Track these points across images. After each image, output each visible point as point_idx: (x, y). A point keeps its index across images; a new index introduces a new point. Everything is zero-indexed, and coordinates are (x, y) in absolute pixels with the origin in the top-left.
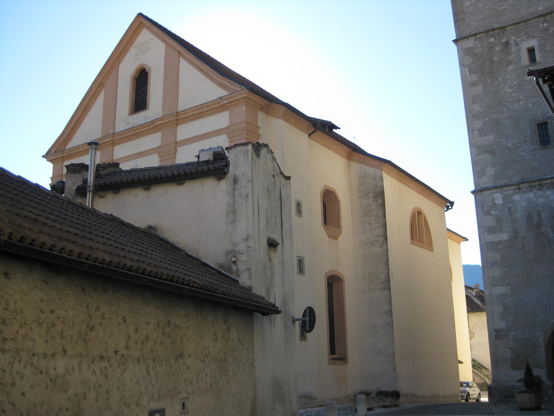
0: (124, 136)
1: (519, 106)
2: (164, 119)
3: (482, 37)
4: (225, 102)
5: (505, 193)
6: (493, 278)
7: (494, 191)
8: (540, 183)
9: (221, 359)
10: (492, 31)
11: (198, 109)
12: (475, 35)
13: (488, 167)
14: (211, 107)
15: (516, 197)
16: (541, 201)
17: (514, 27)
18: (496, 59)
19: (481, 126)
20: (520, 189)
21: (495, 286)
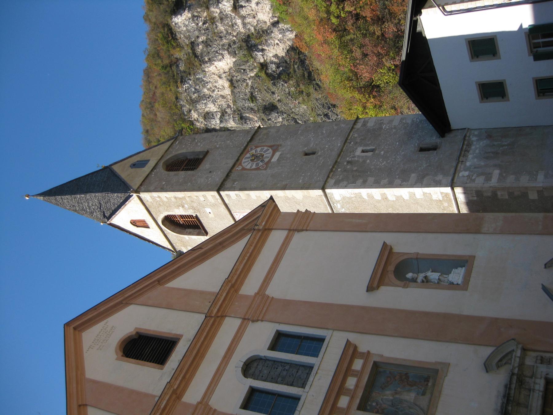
0: (184, 371)
1: (400, 159)
2: (219, 299)
3: (332, 174)
4: (263, 224)
5: (462, 169)
6: (529, 180)
7: (457, 175)
8: (464, 151)
9: (383, 389)
10: (333, 168)
11: (245, 256)
12: (328, 177)
13: (435, 179)
14: (255, 242)
15: (468, 164)
16: (477, 151)
17: (340, 158)
18: (355, 169)
19: (400, 180)
20: (463, 161)
21: (536, 179)
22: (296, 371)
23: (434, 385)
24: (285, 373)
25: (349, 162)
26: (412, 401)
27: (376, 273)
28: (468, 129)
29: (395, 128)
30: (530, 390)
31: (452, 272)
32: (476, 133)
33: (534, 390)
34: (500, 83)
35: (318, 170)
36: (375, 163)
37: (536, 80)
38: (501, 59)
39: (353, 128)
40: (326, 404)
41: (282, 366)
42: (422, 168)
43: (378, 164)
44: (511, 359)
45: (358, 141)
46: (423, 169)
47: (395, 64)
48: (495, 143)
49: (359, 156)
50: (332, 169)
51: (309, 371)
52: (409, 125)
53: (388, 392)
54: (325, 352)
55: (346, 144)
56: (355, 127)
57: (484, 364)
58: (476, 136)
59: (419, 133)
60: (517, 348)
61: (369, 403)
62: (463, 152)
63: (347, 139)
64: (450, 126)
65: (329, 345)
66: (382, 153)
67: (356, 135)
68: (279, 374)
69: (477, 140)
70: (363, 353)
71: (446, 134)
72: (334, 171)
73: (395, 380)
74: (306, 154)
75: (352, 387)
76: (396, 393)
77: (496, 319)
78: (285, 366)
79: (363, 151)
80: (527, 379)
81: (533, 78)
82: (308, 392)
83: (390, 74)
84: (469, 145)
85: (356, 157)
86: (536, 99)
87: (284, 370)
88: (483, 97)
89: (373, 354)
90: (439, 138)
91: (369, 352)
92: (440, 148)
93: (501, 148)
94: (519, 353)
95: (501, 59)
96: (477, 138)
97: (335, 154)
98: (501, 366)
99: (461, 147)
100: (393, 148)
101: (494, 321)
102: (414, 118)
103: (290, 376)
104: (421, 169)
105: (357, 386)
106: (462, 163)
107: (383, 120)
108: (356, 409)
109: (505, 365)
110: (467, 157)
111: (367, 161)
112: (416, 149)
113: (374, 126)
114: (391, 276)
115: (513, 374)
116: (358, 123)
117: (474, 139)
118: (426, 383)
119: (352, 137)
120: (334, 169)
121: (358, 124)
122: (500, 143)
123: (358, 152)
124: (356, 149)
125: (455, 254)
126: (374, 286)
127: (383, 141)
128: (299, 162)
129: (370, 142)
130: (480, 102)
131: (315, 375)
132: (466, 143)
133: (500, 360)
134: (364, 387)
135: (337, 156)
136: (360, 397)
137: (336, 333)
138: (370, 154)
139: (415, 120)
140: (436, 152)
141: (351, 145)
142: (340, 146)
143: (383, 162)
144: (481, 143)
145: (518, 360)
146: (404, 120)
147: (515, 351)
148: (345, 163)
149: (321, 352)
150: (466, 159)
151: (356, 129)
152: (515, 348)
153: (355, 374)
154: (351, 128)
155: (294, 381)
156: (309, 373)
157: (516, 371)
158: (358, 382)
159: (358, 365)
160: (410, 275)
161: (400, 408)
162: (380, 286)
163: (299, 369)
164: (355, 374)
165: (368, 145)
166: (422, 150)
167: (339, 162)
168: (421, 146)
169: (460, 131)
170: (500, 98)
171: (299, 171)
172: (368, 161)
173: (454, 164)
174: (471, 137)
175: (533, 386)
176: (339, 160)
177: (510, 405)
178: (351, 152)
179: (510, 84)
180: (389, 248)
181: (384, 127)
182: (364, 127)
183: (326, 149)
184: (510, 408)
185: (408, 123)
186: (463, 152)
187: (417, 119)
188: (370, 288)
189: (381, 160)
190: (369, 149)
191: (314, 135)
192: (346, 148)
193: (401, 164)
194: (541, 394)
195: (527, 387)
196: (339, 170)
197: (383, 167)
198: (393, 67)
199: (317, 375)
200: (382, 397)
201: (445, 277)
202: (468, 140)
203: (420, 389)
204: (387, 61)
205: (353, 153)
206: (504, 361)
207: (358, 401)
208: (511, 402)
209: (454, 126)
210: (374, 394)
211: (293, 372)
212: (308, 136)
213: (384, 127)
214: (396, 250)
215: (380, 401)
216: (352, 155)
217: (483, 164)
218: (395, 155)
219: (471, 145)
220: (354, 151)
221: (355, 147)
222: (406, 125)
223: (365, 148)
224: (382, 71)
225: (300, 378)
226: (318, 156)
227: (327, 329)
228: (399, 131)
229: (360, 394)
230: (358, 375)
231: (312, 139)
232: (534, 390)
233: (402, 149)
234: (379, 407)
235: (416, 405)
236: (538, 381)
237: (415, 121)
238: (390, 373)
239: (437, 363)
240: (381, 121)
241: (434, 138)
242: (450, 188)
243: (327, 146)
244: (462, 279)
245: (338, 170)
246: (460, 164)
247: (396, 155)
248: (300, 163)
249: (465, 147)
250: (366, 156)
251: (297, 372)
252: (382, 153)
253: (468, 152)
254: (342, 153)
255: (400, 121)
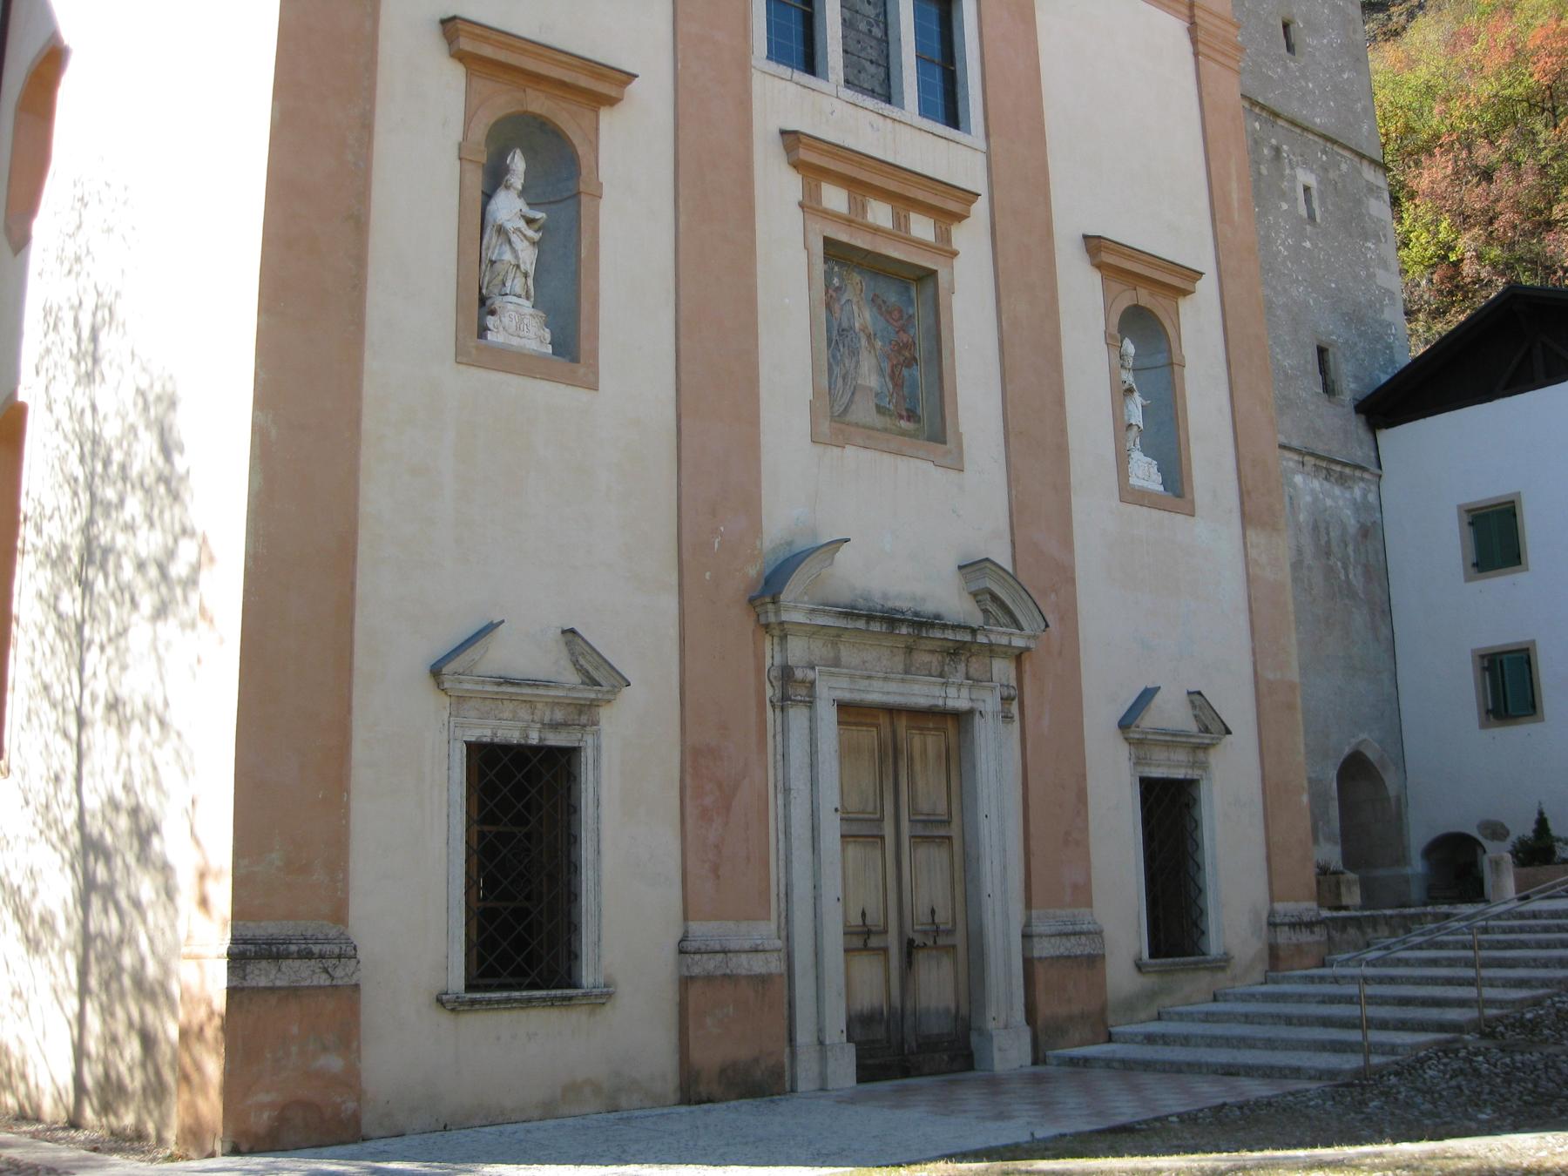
9: (873, 300)
16: (1329, 502)
17: (1286, 125)
18: (1264, 171)
22: (874, 59)
23: (903, 433)
24: (863, 26)
25: (1277, 150)
27: (1133, 257)
28: (1380, 476)
29: (1371, 276)
30: (941, 675)
31: (1149, 460)
32: (1372, 498)
33: (945, 684)
34: (1519, 556)
35: (1250, 64)
36: (1282, 224)
37: (1528, 649)
39: (1362, 156)
40: (828, 152)
41: (878, 15)
42: (1279, 357)
43: (1281, 235)
44: (998, 623)
45: (1332, 175)
46: (1278, 360)
47: (1465, 262)
48: (1350, 549)
49: (1294, 178)
50: (1256, 105)
51: (878, 94)
52: (1378, 316)
53: (867, 315)
54: (935, 135)
55: (1321, 141)
56: (1365, 163)
57: (987, 560)
58: (1365, 496)
59: (1360, 342)
60: (1029, 637)
62: (1330, 466)
63: (1334, 142)
64: (1387, 428)
65: (952, 144)
66: (1308, 244)
67: (1344, 167)
68: (857, 12)
69: (1355, 499)
70: (949, 241)
71: (1363, 417)
72: (1253, 109)
73: (898, 332)
74: (1286, 26)
75: (870, 218)
76: (869, 337)
77: (1072, 581)
78: (878, 25)
79: (1307, 189)
80: (962, 667)
81: (1533, 642)
82: (837, 97)
83: (1433, 248)
84: (1342, 480)
85: (1293, 172)
86: (1473, 651)
87: (869, 23)
88: (1473, 513)
90: (1354, 399)
91: (954, 254)
92: (1330, 401)
93: (1339, 564)
94: (1018, 642)
96: (1359, 500)
97: (1294, 109)
98: (977, 602)
99: (1337, 458)
100: (1320, 274)
101: (1066, 575)
102: (1396, 329)
103: (859, 42)
104: (1277, 354)
105: (876, 230)
106: (1299, 462)
107: (1386, 242)
109: (982, 610)
110: (1315, 476)
111: (1286, 201)
112: (1324, 338)
113: (1370, 215)
114: (1126, 300)
115: (974, 631)
116: (1375, 171)
117: (1357, 492)
118: (904, 413)
119: (1339, 158)
120: (1257, 110)
121: (1373, 172)
122: (1352, 560)
123: (1306, 177)
124: (1312, 171)
125: (1194, 466)
126: (1103, 254)
127: (1336, 244)
128: (1265, 6)
129: (1330, 207)
130: (1459, 507)
131: (880, 112)
132: (1347, 471)
133: (995, 598)
134: (878, 250)
135: (1290, 116)
136: (853, 242)
137: (981, 160)
138: (1302, 210)
139: (1391, 330)
140: (1319, 393)
141: (1319, 154)
142: (1315, 124)
143: (1285, 249)
144: (1349, 512)
145: (1004, 641)
146: (1389, 300)
147: (1023, 633)
148: (1274, 141)
149: (933, 122)
150: (1308, 474)
151: (1358, 165)
152: (1028, 631)
153: (901, 222)
154: (1361, 151)
155: (849, 55)
156: (875, 95)
157: (981, 639)
159: (922, 227)
160: (1129, 347)
161: (839, 351)
162: (1100, 271)
163: (879, 65)
164: (901, 222)
165: (1323, 203)
166: (1322, 351)
167: (1277, 124)
168: (1331, 350)
169: (1373, 454)
170: (1472, 558)
171: (1245, 9)
172: (1285, 206)
173: (1295, 443)
174: (1362, 485)
175: (953, 683)
176: (1280, 122)
177: (911, 630)
178: (1302, 156)
179: (1514, 584)
180: (1189, 288)
181: (1369, 244)
182: (1365, 190)
183: (1303, 83)
184: (904, 630)
185: (1383, 312)
186: (1324, 464)
187: (1394, 336)
188: (1094, 245)
189: (1289, 240)
190: (1314, 206)
191: (1334, 45)
192: (1311, 143)
193: (1285, 300)
194: (940, 702)
195: (946, 668)
196: (1257, 125)
197: (1274, 248)
198: (1453, 258)
199: (881, 118)
201: (1135, 441)
202: (1354, 475)
204: (1475, 239)
205: (1300, 163)
206: (992, 608)
207: (843, 237)
208: (916, 632)
209: (1387, 437)
210: (856, 277)
211: (869, 50)
212: (1332, 29)
213: (1369, 244)
214: (1184, 305)
216: (1295, 160)
217: (1301, 518)
218: (1306, 281)
219: (1342, 484)
220: (1306, 164)
221: (1314, 167)
222: (1378, 305)
223: (1314, 193)
224: (1445, 228)
225: (860, 72)
226: (1285, 62)
227: (987, 136)
228: (1363, 288)
229: (861, 241)
230: (900, 233)
231: (1325, 41)
232: (945, 684)
233: (1321, 298)
236: (965, 692)
237: (1389, 332)
238: (910, 316)
239: (959, 436)
240: (1385, 236)
241: (1352, 386)
243: (1311, 85)
244: (1139, 486)
245: (1256, 121)
246: (1296, 457)
247: (1305, 284)
248: (1264, 8)
249: (1338, 468)
250: (1297, 199)
251: (872, 62)
252: (1308, 244)
253: (1326, 479)
254: (1298, 131)
255: (1387, 290)
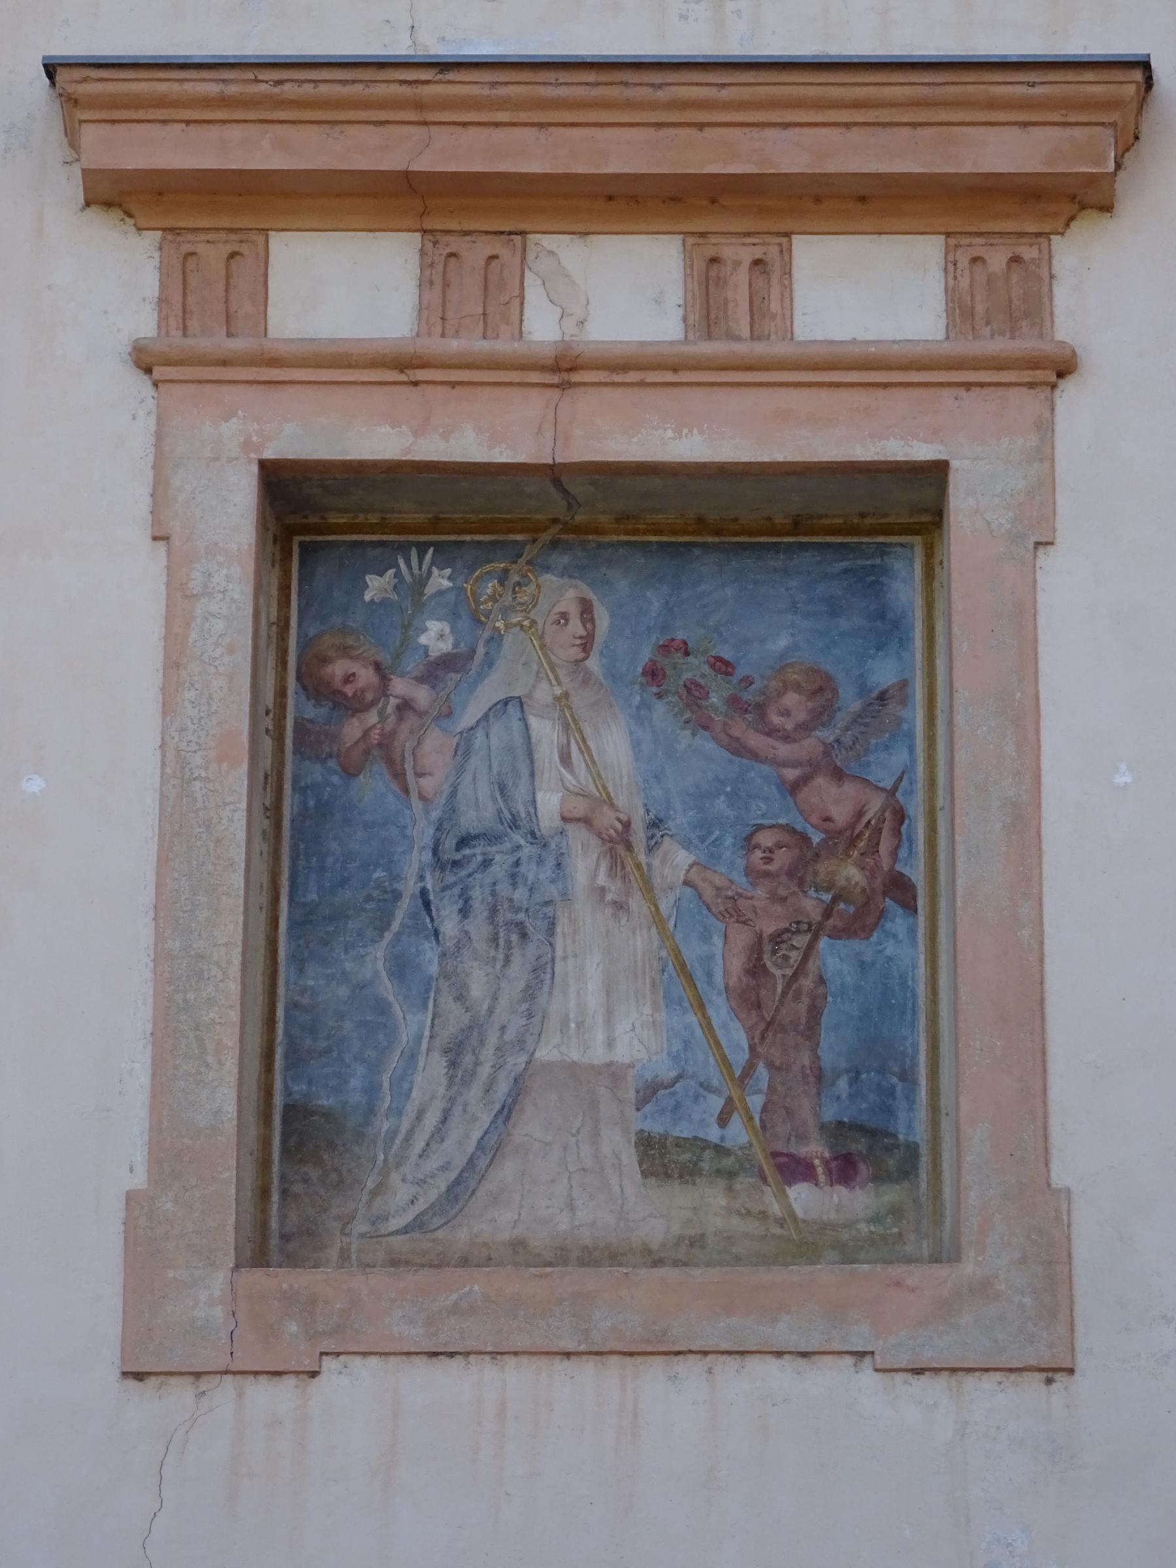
26: (545, 1053)
38: (263, 465)
61: (440, 580)
73: (794, 788)
89: (1046, 427)
95: (263, 465)
108: (269, 454)
118: (815, 1149)
158: (624, 366)
200: (544, 693)
203: (716, 1103)
215: (487, 694)
234: (405, 706)
235: (506, 1113)
242: (276, 240)
